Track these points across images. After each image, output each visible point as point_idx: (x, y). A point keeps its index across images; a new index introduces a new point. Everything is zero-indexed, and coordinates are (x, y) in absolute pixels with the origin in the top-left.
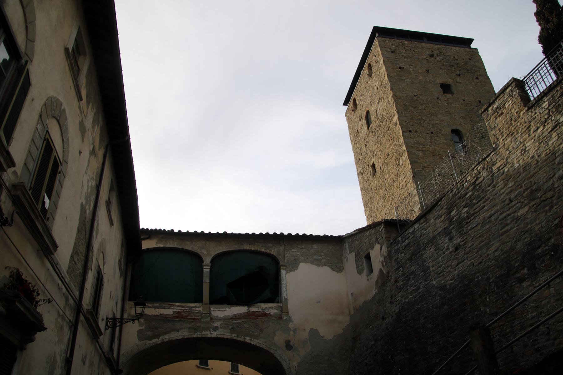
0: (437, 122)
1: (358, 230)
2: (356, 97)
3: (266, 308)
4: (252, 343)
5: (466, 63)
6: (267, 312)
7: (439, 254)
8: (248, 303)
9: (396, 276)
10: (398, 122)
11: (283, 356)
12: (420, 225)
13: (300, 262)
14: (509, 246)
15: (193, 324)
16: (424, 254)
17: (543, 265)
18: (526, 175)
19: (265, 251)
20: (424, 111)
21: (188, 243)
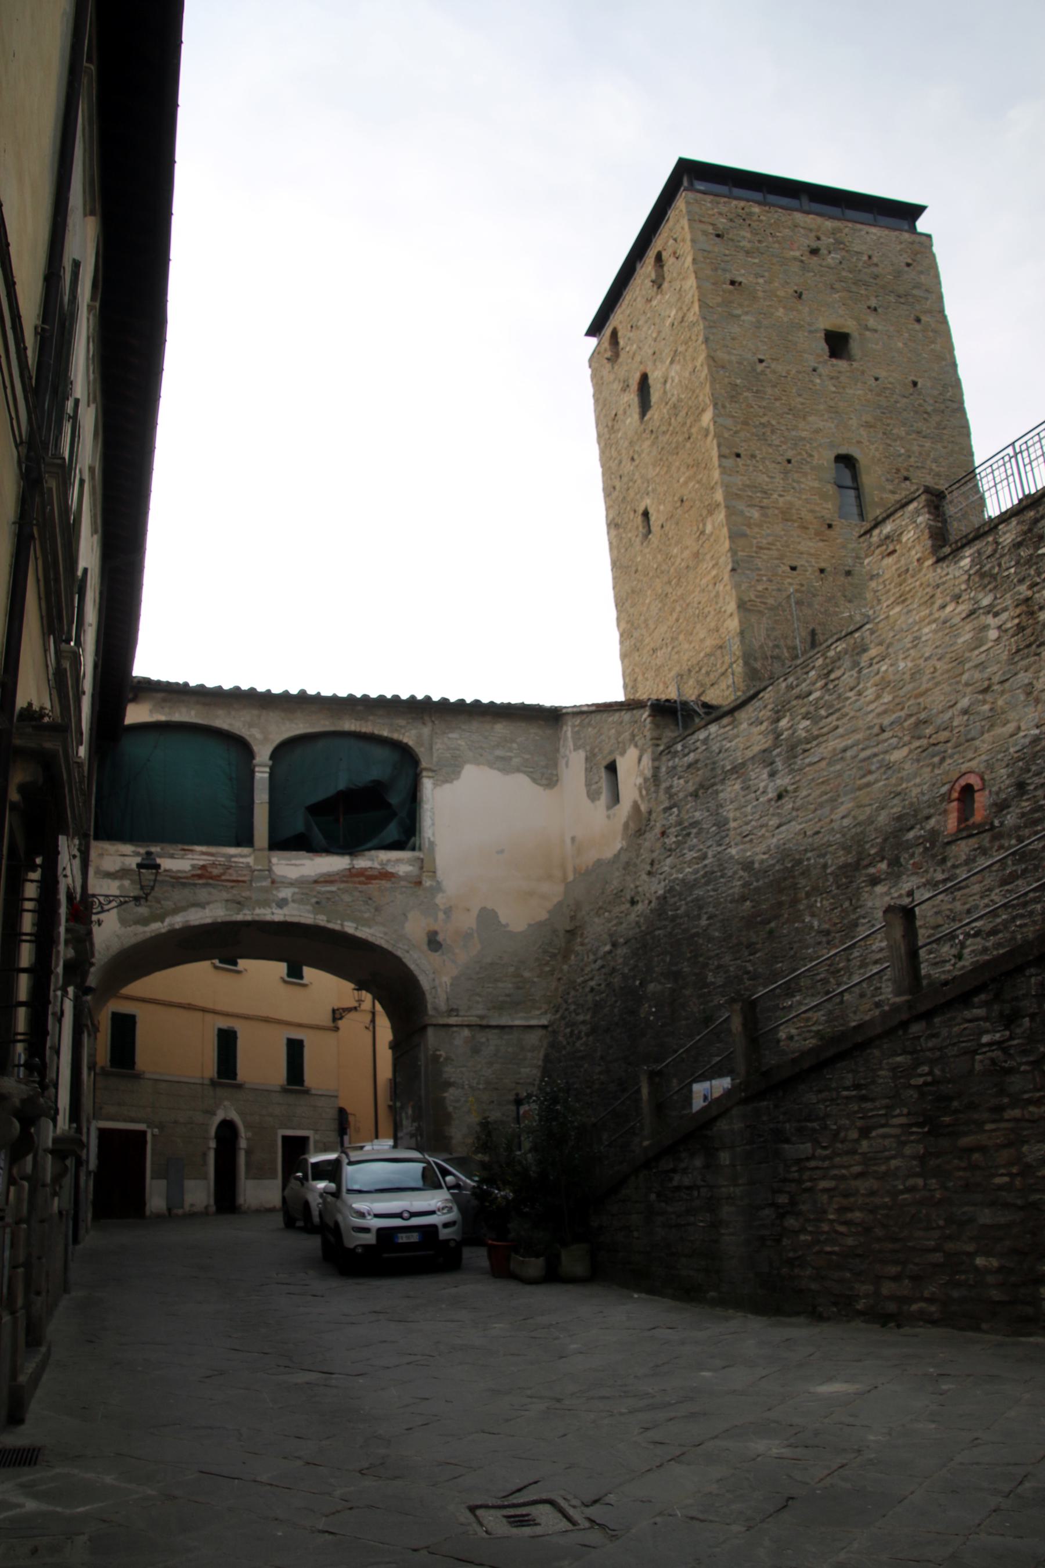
0: (804, 434)
1: (597, 705)
2: (620, 328)
3: (389, 861)
4: (359, 934)
5: (898, 274)
6: (390, 869)
7: (748, 798)
8: (350, 846)
9: (665, 822)
10: (712, 428)
11: (421, 963)
12: (720, 728)
13: (466, 762)
14: (868, 812)
15: (235, 892)
16: (722, 791)
17: (911, 862)
18: (914, 689)
19: (390, 735)
20: (778, 404)
21: (220, 712)
